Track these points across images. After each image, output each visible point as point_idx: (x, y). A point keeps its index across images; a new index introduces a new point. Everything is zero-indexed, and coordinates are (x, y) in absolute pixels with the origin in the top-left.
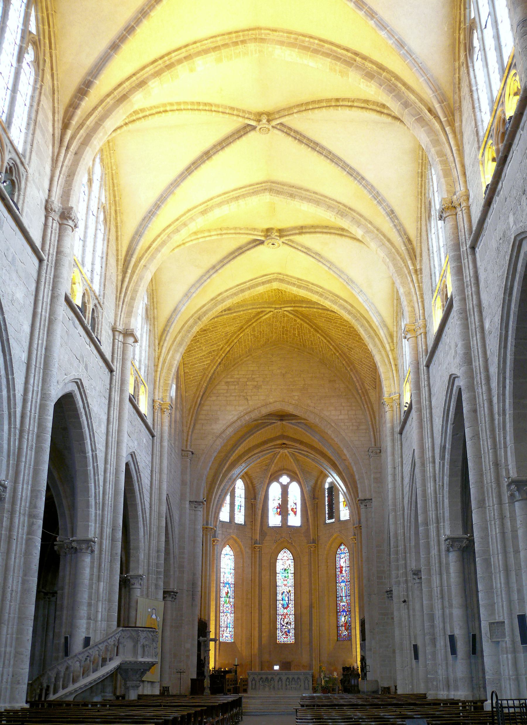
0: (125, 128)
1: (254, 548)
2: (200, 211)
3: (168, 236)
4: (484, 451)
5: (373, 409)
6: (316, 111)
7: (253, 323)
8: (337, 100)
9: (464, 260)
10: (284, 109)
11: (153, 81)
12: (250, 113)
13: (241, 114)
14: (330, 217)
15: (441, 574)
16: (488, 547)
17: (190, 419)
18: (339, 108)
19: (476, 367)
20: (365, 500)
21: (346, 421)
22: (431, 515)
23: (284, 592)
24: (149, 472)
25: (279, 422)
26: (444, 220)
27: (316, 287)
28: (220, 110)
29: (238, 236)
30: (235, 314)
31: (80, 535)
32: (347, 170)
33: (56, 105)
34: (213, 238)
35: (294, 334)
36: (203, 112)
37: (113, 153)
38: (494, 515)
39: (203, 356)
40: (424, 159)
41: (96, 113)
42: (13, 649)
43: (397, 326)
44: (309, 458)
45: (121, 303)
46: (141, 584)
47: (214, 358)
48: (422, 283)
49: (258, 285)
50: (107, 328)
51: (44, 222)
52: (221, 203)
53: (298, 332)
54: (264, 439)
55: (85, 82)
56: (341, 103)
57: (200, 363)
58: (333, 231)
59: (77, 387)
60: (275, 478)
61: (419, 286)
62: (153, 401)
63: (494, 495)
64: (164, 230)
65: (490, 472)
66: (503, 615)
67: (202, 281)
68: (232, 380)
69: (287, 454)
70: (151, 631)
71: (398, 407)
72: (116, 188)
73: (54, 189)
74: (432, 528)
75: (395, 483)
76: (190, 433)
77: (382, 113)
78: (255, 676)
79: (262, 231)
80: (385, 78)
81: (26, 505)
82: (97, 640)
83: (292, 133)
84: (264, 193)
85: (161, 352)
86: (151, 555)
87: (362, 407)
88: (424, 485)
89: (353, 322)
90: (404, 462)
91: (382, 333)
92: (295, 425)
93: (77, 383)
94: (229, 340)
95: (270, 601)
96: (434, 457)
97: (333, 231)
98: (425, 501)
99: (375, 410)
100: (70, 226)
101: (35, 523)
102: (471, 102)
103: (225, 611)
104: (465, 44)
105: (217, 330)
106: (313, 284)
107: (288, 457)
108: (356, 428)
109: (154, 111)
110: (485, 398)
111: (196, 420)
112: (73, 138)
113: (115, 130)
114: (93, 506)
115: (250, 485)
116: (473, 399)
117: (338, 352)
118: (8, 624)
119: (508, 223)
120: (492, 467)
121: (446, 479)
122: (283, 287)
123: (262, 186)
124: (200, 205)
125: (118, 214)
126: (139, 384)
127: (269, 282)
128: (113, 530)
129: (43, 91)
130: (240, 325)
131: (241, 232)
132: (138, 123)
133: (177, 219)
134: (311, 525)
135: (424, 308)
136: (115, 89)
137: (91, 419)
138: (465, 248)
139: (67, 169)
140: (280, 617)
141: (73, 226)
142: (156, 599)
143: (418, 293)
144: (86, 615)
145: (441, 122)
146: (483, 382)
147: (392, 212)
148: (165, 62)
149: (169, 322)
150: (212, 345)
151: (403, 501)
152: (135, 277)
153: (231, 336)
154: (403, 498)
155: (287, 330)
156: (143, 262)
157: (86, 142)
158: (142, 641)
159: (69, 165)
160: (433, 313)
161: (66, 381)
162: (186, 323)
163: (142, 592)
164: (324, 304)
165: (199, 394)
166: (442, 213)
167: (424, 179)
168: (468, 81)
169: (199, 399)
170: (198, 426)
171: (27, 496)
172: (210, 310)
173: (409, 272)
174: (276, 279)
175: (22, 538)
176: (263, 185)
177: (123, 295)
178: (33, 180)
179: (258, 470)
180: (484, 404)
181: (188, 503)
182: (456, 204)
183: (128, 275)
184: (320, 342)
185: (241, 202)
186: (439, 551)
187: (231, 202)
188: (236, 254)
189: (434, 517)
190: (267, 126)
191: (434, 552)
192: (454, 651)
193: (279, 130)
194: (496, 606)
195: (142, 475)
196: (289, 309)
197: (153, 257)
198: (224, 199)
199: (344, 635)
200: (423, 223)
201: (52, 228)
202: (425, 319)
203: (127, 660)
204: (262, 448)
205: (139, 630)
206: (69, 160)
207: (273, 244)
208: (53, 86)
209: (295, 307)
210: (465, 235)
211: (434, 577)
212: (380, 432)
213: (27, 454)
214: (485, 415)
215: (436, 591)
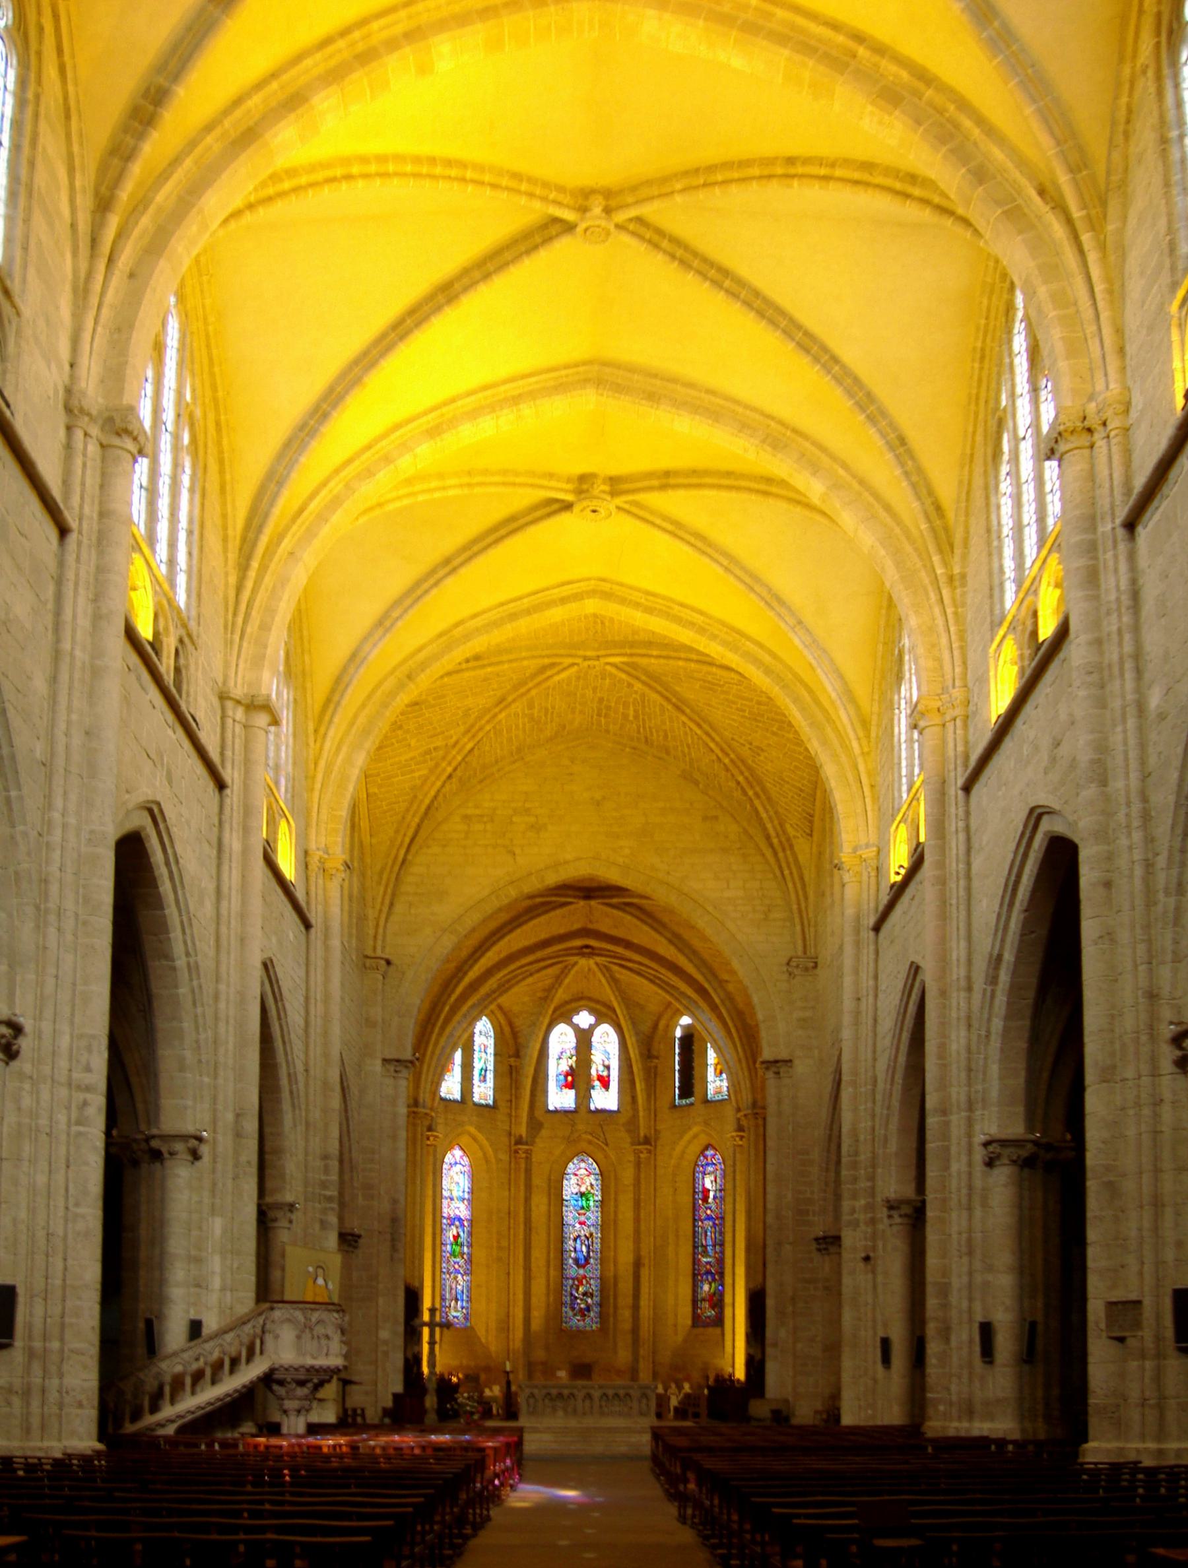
0: (248, 217)
1: (516, 1152)
3: (347, 486)
5: (802, 878)
6: (733, 188)
8: (791, 161)
10: (648, 183)
11: (323, 94)
12: (561, 189)
13: (538, 192)
14: (746, 450)
17: (381, 892)
18: (796, 183)
20: (776, 1062)
23: (579, 1236)
24: (302, 999)
25: (582, 903)
26: (1060, 460)
27: (688, 611)
28: (487, 178)
29: (510, 490)
30: (489, 669)
32: (797, 339)
33: (76, 149)
34: (451, 493)
35: (625, 716)
36: (442, 184)
37: (209, 282)
39: (412, 759)
41: (179, 174)
45: (237, 637)
47: (437, 765)
50: (208, 690)
54: (543, 936)
55: (148, 90)
56: (800, 170)
58: (743, 483)
59: (149, 820)
60: (564, 1014)
62: (306, 853)
64: (337, 471)
67: (419, 592)
68: (478, 812)
72: (216, 369)
73: (84, 361)
75: (857, 1030)
76: (382, 923)
77: (907, 196)
78: (536, 1391)
79: (569, 480)
80: (930, 104)
85: (321, 749)
89: (776, 691)
91: (843, 717)
93: (151, 811)
94: (472, 726)
95: (549, 1253)
97: (743, 483)
99: (806, 879)
100: (130, 452)
102: (1160, 169)
103: (452, 1269)
104: (1159, 15)
106: (682, 605)
107: (594, 974)
108: (762, 916)
109: (319, 176)
111: (394, 895)
113: (226, 221)
115: (507, 1029)
117: (727, 755)
122: (611, 609)
123: (578, 373)
124: (425, 413)
125: (224, 432)
126: (277, 816)
127: (578, 597)
129: (42, 111)
130: (499, 694)
131: (518, 480)
132: (280, 204)
133: (369, 447)
134: (641, 1109)
135: (965, 663)
136: (227, 111)
137: (183, 887)
140: (571, 1282)
141: (135, 451)
143: (952, 629)
145: (1069, 221)
147: (902, 441)
148: (353, 44)
149: (340, 683)
150: (431, 737)
152: (268, 580)
153: (479, 718)
155: (608, 708)
156: (286, 544)
157: (157, 246)
160: (992, 673)
161: (131, 806)
165: (402, 842)
166: (1056, 442)
168: (1156, 114)
169: (402, 852)
170: (399, 908)
172: (436, 657)
174: (592, 593)
176: (581, 369)
177: (240, 620)
179: (526, 999)
181: (379, 1062)
182: (1093, 422)
183: (252, 574)
184: (686, 734)
185: (527, 410)
187: (502, 409)
188: (503, 532)
190: (603, 223)
193: (634, 234)
195: (288, 1006)
196: (616, 660)
197: (310, 534)
200: (978, 470)
201: (85, 455)
202: (966, 686)
204: (539, 954)
207: (594, 511)
208: (66, 98)
209: (631, 655)
212: (816, 925)
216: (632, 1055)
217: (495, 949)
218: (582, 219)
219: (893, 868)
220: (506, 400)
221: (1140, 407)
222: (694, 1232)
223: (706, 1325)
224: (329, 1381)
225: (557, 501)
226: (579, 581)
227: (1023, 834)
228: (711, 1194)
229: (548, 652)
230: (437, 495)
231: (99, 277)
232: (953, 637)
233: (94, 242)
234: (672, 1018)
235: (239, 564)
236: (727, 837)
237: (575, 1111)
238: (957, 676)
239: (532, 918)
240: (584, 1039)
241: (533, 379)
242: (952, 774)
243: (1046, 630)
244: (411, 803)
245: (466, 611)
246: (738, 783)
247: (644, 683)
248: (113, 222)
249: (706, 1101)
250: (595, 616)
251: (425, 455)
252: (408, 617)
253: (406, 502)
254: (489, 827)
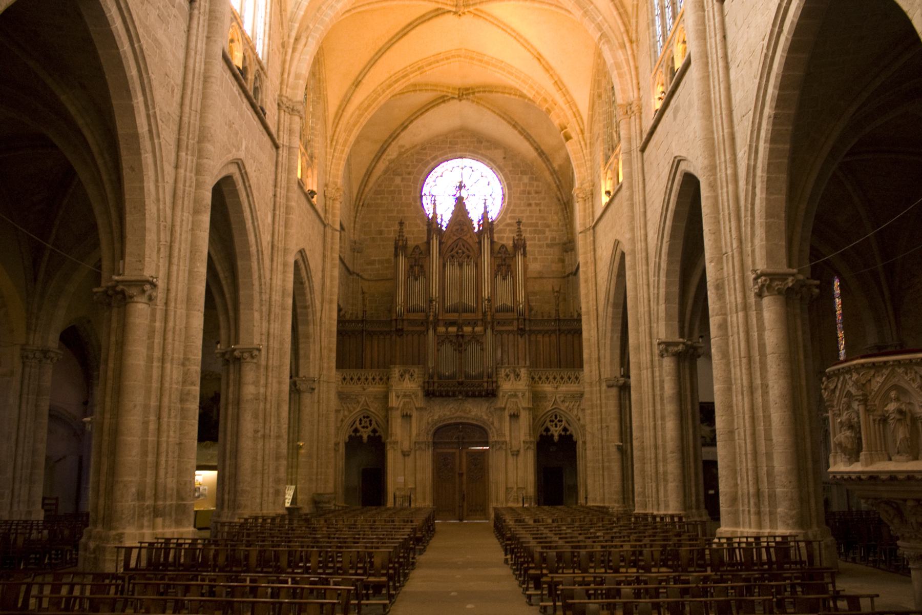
93: (237, 163)
243: (678, 65)
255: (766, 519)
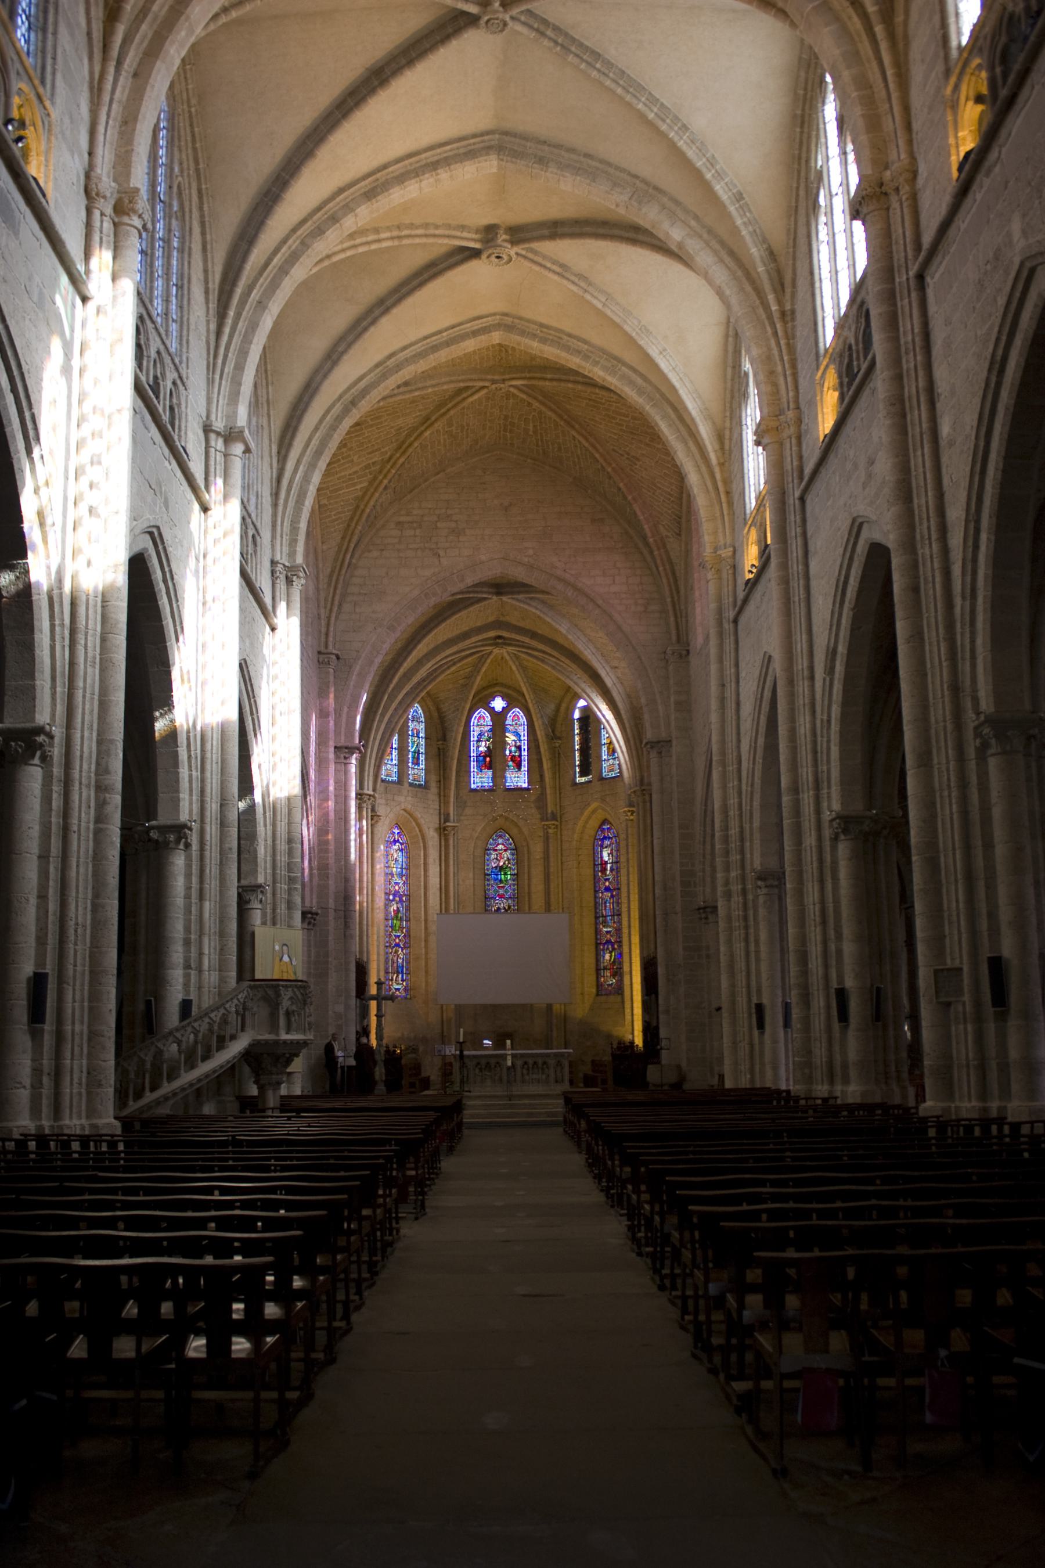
1: (445, 829)
2: (363, 190)
3: (303, 243)
4: (932, 663)
5: (674, 573)
7: (449, 410)
9: (902, 300)
15: (822, 881)
16: (936, 837)
19: (919, 506)
20: (659, 742)
21: (624, 596)
22: (804, 774)
25: (495, 597)
27: (575, 341)
30: (417, 393)
31: (163, 818)
34: (385, 244)
38: (949, 779)
39: (356, 472)
40: (809, 88)
42: (85, 1028)
43: (731, 418)
44: (546, 663)
45: (217, 377)
46: (261, 901)
48: (793, 338)
49: (463, 337)
50: (195, 425)
51: (85, 220)
52: (402, 175)
53: (534, 426)
57: (347, 487)
59: (151, 542)
61: (788, 345)
63: (950, 743)
64: (294, 230)
65: (943, 702)
66: (961, 956)
67: (360, 329)
68: (409, 519)
69: (506, 655)
70: (301, 987)
71: (730, 572)
73: (99, 151)
74: (807, 798)
79: (477, 232)
81: (90, 768)
82: (205, 1005)
83: (549, 33)
84: (488, 154)
86: (278, 847)
87: (654, 569)
88: (792, 719)
90: (743, 674)
92: (524, 603)
93: (151, 534)
94: (403, 442)
96: (811, 668)
98: (794, 749)
100: (136, 228)
101: (108, 800)
105: (381, 423)
106: (570, 335)
110: (936, 565)
112: (127, 41)
114: (186, 763)
115: (436, 714)
116: (913, 567)
118: (74, 985)
119: (1009, 235)
120: (946, 693)
121: (836, 710)
122: (514, 340)
123: (483, 142)
124: (364, 178)
125: (205, 199)
128: (221, 805)
131: (437, 232)
133: (319, 209)
134: (548, 786)
138: (905, 277)
139: (121, 109)
141: (140, 227)
142: (290, 926)
143: (786, 358)
144: (181, 961)
146: (934, 536)
151: (738, 747)
153: (409, 435)
154: (739, 741)
158: (285, 1004)
159: (124, 99)
160: (818, 398)
162: (328, 411)
163: (264, 915)
164: (590, 375)
167: (806, 130)
169: (348, 556)
171: (91, 752)
173: (770, 317)
174: (498, 326)
175: (88, 828)
176: (486, 138)
177: (220, 361)
178: (63, 133)
180: (933, 576)
181: (332, 749)
183: (229, 321)
185: (443, 174)
186: (820, 839)
187: (423, 174)
188: (426, 276)
189: (810, 778)
191: (810, 840)
192: (843, 1016)
193: (524, 24)
194: (947, 940)
198: (409, 168)
199: (609, 985)
201: (101, 232)
203: (260, 1037)
205: (278, 985)
206: (124, 88)
210: (905, 251)
211: (810, 885)
212: (687, 617)
213: (85, 673)
214: (935, 597)
215: (813, 911)
216: (539, 737)
217: (425, 641)
218: (484, 13)
219: (747, 568)
220: (426, 165)
221: (925, 174)
222: (596, 903)
223: (608, 994)
224: (297, 1055)
225: (468, 248)
226: (487, 316)
227: (848, 540)
228: (609, 866)
229: (463, 377)
230: (374, 247)
231: (110, 78)
232: (787, 366)
233: (106, 48)
234: (570, 702)
235: (218, 312)
236: (612, 537)
237: (491, 790)
238: (791, 400)
239: (454, 614)
240: (499, 719)
241: (448, 148)
242: (791, 485)
244: (355, 513)
245: (397, 345)
246: (619, 489)
247: (541, 403)
248: (121, 30)
249: (602, 779)
250: (500, 345)
251: (364, 215)
252: (352, 352)
253: (349, 253)
254: (418, 532)
255: (74, 1116)
